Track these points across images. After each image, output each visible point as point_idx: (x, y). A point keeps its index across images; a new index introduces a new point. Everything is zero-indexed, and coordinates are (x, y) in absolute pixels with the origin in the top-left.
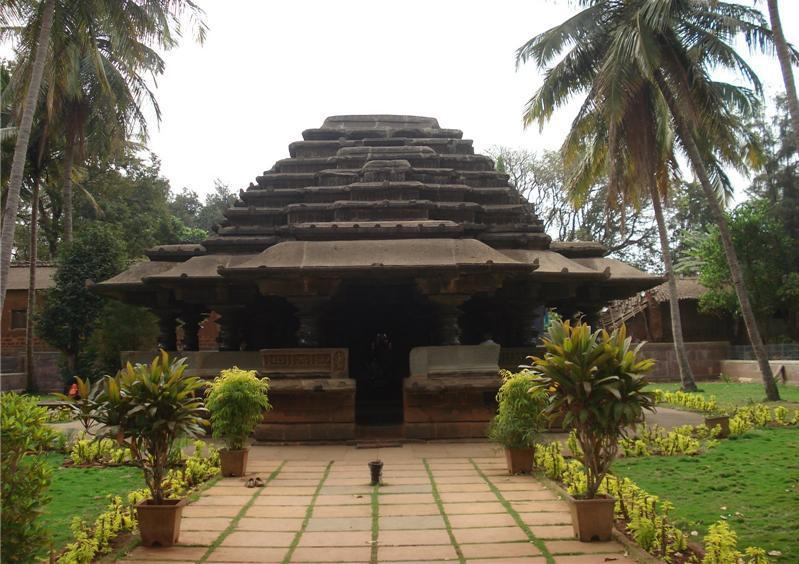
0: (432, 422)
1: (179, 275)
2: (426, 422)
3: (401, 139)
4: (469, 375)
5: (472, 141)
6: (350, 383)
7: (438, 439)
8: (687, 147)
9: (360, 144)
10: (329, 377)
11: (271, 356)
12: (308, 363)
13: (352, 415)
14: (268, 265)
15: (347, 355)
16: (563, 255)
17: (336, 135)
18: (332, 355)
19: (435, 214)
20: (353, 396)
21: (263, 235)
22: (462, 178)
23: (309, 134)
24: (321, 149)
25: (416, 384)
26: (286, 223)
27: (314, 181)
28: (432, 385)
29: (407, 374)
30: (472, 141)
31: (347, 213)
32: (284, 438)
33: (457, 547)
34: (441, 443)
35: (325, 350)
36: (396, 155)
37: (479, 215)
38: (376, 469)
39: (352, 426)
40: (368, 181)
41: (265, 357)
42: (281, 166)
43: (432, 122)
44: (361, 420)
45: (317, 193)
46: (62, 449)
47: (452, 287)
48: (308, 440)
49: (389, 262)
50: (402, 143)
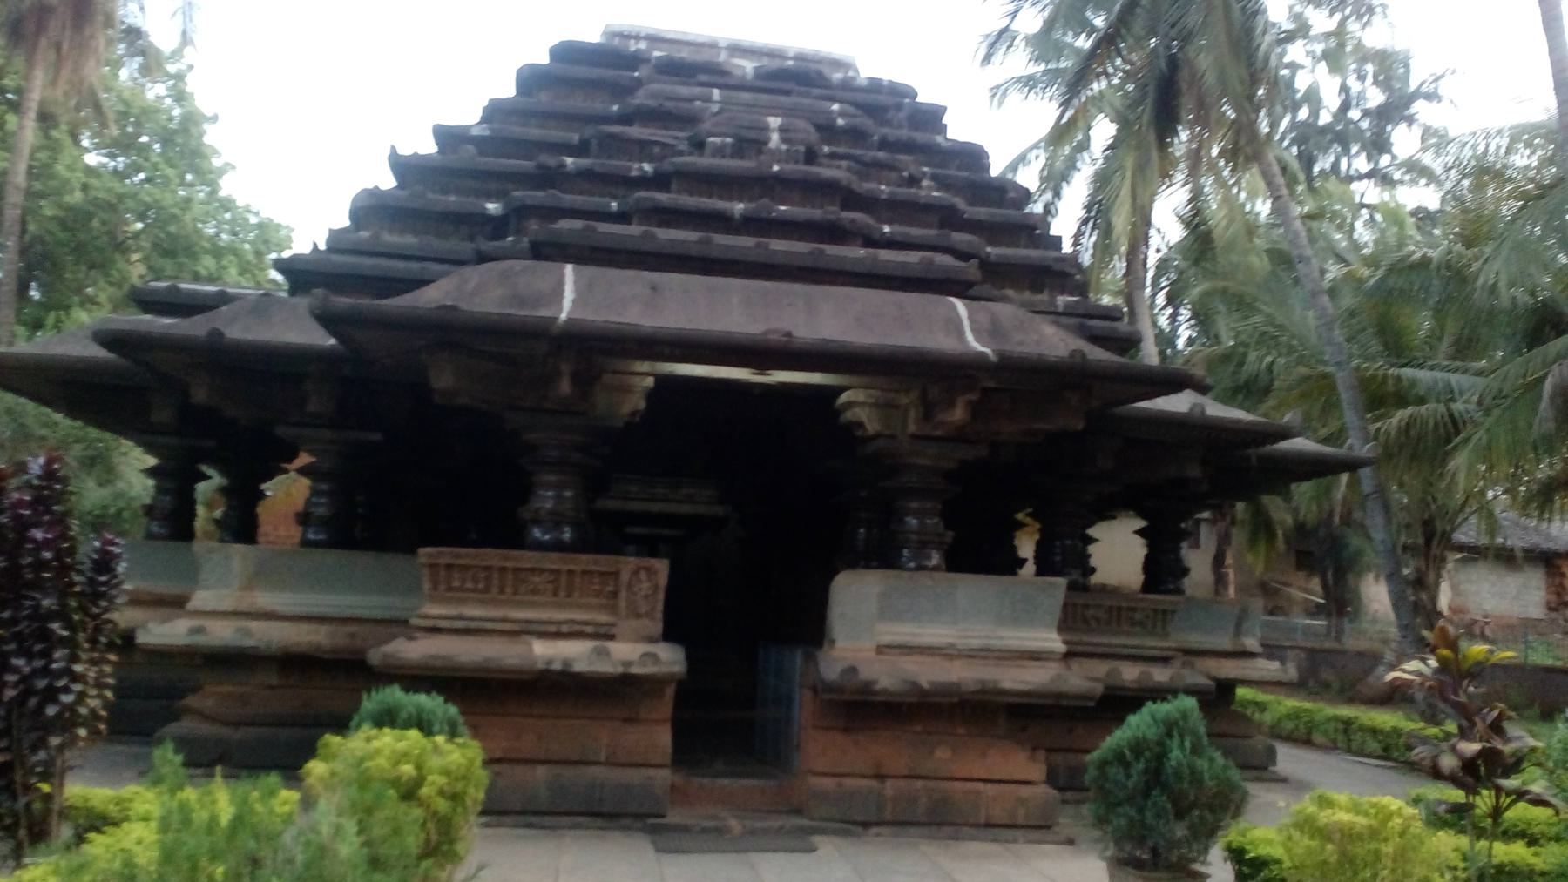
0: (881, 777)
2: (863, 776)
5: (945, 109)
6: (670, 659)
8: (1134, 402)
10: (611, 637)
11: (449, 567)
13: (664, 737)
15: (663, 580)
18: (625, 577)
20: (670, 691)
23: (566, 53)
25: (852, 670)
28: (886, 676)
30: (945, 109)
32: (602, 758)
34: (770, 49)
35: (603, 562)
39: (664, 776)
41: (433, 566)
45: (586, 175)
49: (703, 206)
50: (788, 93)
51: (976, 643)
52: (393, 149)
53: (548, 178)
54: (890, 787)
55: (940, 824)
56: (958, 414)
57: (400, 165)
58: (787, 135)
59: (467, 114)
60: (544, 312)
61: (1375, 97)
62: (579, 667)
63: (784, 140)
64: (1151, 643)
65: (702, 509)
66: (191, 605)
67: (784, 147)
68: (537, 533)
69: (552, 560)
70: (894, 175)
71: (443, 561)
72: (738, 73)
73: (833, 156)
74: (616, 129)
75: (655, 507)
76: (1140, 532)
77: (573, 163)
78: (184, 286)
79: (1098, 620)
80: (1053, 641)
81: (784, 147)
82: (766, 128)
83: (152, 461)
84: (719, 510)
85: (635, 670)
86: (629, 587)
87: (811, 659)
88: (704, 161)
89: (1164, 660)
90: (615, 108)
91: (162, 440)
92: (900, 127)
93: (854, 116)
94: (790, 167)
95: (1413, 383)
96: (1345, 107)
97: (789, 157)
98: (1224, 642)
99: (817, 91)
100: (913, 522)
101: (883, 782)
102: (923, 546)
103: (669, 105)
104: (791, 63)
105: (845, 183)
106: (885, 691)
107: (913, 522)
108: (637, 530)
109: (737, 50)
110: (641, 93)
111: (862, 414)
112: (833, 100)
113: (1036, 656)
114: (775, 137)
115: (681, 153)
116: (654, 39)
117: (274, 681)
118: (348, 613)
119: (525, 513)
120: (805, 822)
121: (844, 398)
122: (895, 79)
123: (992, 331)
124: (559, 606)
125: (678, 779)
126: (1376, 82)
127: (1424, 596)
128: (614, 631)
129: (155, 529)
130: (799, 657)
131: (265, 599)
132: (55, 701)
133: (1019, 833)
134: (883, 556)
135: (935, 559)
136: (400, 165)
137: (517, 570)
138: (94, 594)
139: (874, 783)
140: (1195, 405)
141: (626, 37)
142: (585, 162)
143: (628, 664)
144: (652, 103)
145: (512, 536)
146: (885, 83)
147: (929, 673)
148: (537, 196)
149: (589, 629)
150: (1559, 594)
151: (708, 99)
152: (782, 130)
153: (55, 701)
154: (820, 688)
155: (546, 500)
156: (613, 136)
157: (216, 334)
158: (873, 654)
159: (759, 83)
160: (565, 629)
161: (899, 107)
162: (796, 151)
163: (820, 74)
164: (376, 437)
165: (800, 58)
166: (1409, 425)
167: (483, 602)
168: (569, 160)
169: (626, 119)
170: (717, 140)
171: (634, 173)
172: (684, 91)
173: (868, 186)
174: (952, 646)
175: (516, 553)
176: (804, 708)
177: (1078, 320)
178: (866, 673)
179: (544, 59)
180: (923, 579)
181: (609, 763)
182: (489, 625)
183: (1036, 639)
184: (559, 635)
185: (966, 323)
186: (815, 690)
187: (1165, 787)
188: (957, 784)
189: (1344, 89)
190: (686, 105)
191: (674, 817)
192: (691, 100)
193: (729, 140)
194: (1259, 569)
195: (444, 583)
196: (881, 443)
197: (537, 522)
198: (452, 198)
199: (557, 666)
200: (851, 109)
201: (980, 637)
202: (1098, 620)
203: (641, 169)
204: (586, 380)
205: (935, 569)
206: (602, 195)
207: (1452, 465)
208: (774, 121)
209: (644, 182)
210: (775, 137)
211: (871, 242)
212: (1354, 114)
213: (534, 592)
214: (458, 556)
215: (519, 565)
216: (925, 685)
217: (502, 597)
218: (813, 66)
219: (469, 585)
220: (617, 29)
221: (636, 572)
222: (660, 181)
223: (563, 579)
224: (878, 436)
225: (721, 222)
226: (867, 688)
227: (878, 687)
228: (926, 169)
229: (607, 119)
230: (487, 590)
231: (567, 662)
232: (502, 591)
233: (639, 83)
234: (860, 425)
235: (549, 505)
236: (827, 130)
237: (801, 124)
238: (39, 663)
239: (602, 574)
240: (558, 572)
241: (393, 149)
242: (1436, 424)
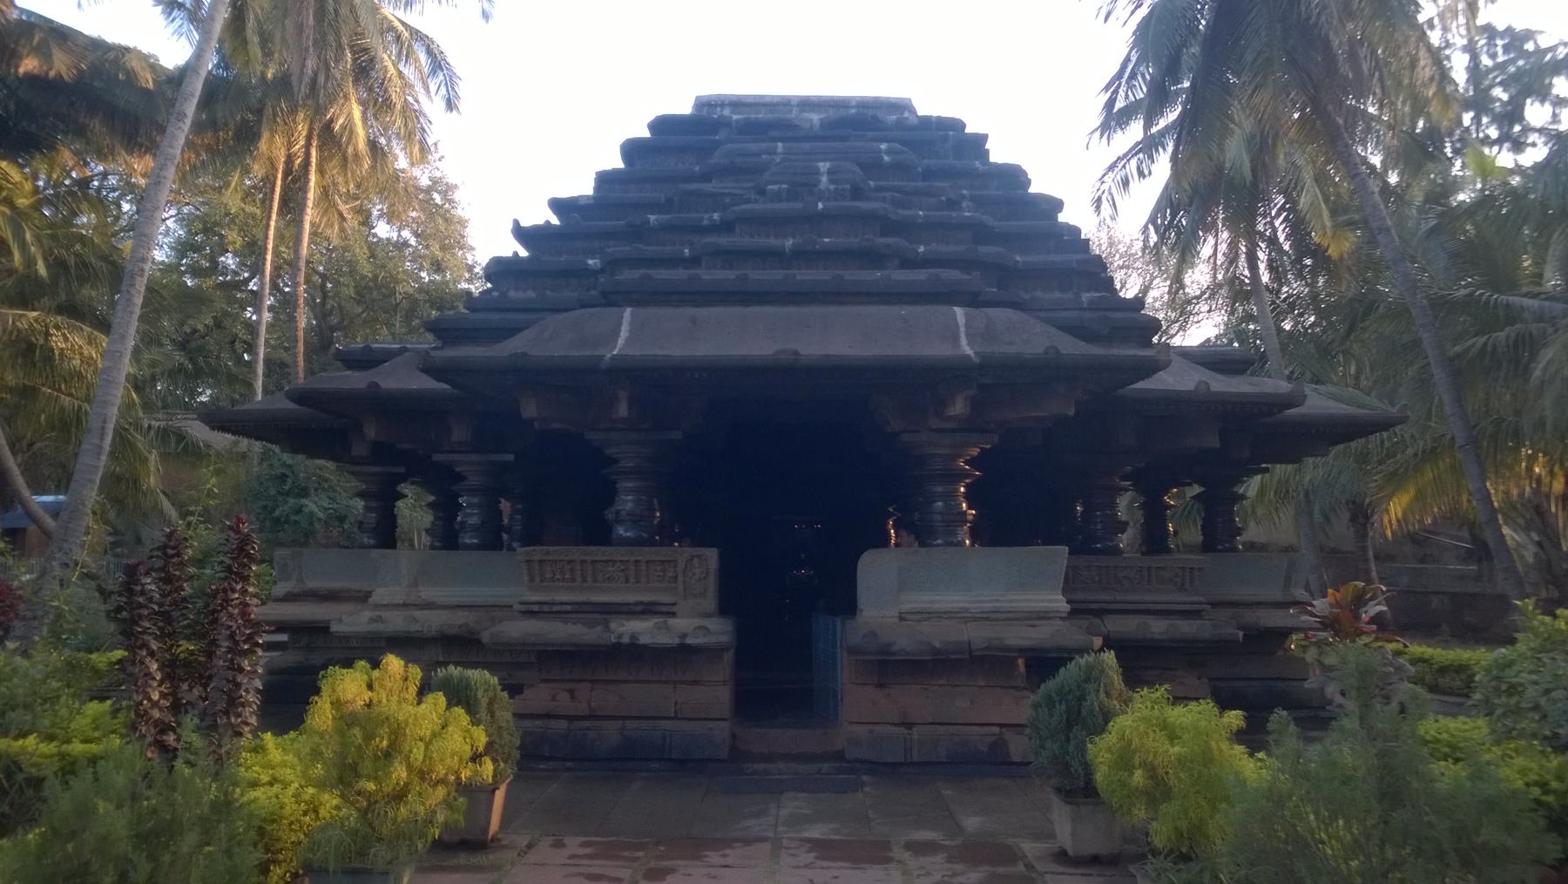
0: (909, 726)
10: (673, 615)
12: (627, 581)
16: (1206, 368)
18: (681, 565)
20: (729, 657)
23: (663, 125)
28: (903, 642)
29: (849, 607)
35: (662, 553)
36: (806, 275)
40: (772, 201)
43: (902, 106)
46: (1319, 647)
47: (958, 408)
50: (844, 139)
52: (516, 223)
53: (637, 233)
57: (522, 234)
59: (583, 186)
63: (831, 181)
66: (374, 599)
67: (832, 187)
68: (621, 531)
71: (537, 557)
73: (879, 189)
74: (694, 186)
77: (656, 220)
80: (1060, 603)
81: (832, 187)
82: (817, 172)
85: (689, 641)
88: (761, 206)
91: (365, 469)
94: (831, 204)
98: (1276, 595)
99: (870, 134)
101: (910, 729)
104: (853, 111)
113: (1044, 616)
114: (824, 179)
115: (748, 201)
119: (610, 515)
122: (944, 114)
128: (675, 609)
129: (437, 544)
130: (838, 621)
131: (428, 593)
134: (921, 533)
136: (522, 234)
137: (593, 562)
139: (903, 730)
140: (1200, 382)
142: (665, 217)
143: (684, 636)
145: (599, 533)
146: (934, 120)
147: (940, 635)
155: (627, 502)
157: (374, 386)
158: (897, 620)
161: (945, 139)
162: (843, 189)
163: (875, 118)
164: (511, 457)
168: (652, 218)
169: (706, 177)
170: (775, 187)
171: (706, 222)
172: (754, 147)
174: (966, 610)
179: (645, 133)
183: (1043, 601)
185: (962, 329)
192: (758, 155)
193: (785, 186)
201: (990, 601)
203: (710, 219)
208: (824, 166)
209: (714, 229)
210: (824, 179)
211: (908, 263)
214: (548, 553)
215: (596, 559)
216: (937, 645)
217: (585, 585)
218: (871, 112)
222: (727, 227)
225: (774, 256)
227: (895, 648)
228: (965, 192)
229: (692, 178)
230: (573, 580)
231: (633, 636)
232: (584, 580)
233: (718, 144)
235: (629, 506)
241: (516, 223)
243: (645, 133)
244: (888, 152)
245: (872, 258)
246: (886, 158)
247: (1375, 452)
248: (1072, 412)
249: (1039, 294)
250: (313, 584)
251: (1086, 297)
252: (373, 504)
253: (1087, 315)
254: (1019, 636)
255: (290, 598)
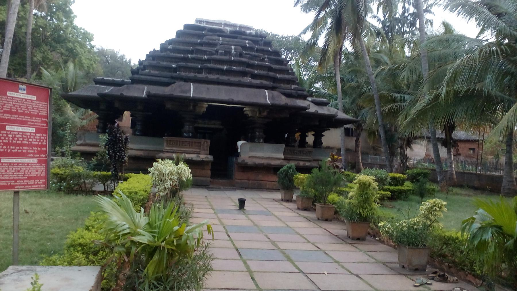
0: (249, 180)
1: (314, 111)
3: (236, 35)
4: (269, 158)
6: (211, 158)
7: (257, 188)
9: (214, 35)
10: (200, 154)
13: (209, 172)
14: (174, 94)
15: (209, 144)
17: (203, 29)
18: (202, 143)
19: (254, 76)
20: (210, 164)
21: (163, 77)
22: (266, 59)
23: (187, 27)
24: (193, 35)
25: (244, 161)
26: (373, 95)
27: (191, 52)
28: (250, 162)
31: (211, 71)
33: (232, 241)
37: (275, 80)
38: (242, 203)
39: (209, 179)
41: (167, 141)
42: (170, 42)
44: (213, 176)
45: (193, 59)
48: (198, 185)
50: (236, 38)
51: (267, 156)
54: (250, 182)
55: (259, 189)
56: (265, 114)
58: (236, 50)
60: (188, 95)
61: (412, 10)
62: (194, 159)
63: (235, 51)
64: (307, 158)
65: (217, 127)
69: (188, 140)
70: (259, 59)
71: (169, 139)
72: (226, 31)
73: (246, 54)
75: (206, 126)
76: (313, 135)
78: (105, 78)
79: (296, 153)
80: (282, 156)
81: (235, 53)
82: (232, 49)
83: (97, 116)
84: (221, 127)
85: (204, 160)
86: (203, 145)
87: (237, 159)
89: (309, 161)
90: (199, 41)
92: (261, 45)
93: (251, 44)
95: (396, 97)
96: (404, 12)
97: (235, 56)
99: (244, 37)
100: (257, 133)
102: (259, 138)
103: (210, 41)
104: (238, 29)
105: (247, 62)
106: (250, 164)
107: (257, 133)
108: (200, 131)
109: (226, 25)
110: (204, 38)
111: (248, 112)
112: (246, 39)
113: (279, 159)
114: (233, 51)
116: (208, 22)
117: (132, 162)
118: (147, 149)
120: (235, 187)
121: (245, 109)
123: (272, 98)
124: (190, 148)
125: (212, 180)
126: (413, 6)
127: (402, 151)
132: (124, 159)
133: (274, 190)
135: (262, 141)
137: (182, 141)
138: (125, 143)
141: (200, 21)
143: (202, 159)
144: (207, 41)
145: (180, 135)
147: (258, 161)
148: (183, 64)
149: (196, 152)
150: (457, 152)
151: (219, 40)
152: (235, 49)
153: (124, 159)
154: (238, 164)
155: (187, 128)
156: (199, 50)
159: (231, 35)
160: (191, 152)
163: (244, 32)
164: (151, 114)
165: (240, 27)
166: (391, 108)
167: (176, 147)
168: (189, 55)
170: (221, 51)
171: (203, 59)
173: (252, 62)
174: (263, 157)
175: (182, 138)
176: (235, 168)
177: (296, 91)
178: (246, 161)
179: (182, 28)
180: (258, 145)
181: (199, 176)
182: (169, 151)
184: (190, 153)
186: (237, 164)
187: (288, 177)
188: (263, 182)
189: (404, 7)
190: (214, 42)
191: (211, 186)
192: (215, 40)
194: (371, 143)
195: (169, 143)
196: (251, 118)
197: (185, 132)
198: (165, 63)
199: (190, 159)
200: (250, 42)
202: (296, 153)
204: (194, 106)
205: (262, 142)
206: (197, 63)
207: (398, 119)
208: (233, 47)
210: (233, 51)
212: (406, 15)
213: (185, 145)
219: (173, 144)
220: (199, 20)
221: (204, 142)
223: (191, 143)
224: (251, 117)
226: (246, 164)
230: (177, 145)
231: (192, 158)
234: (248, 114)
235: (187, 129)
236: (244, 48)
237: (239, 47)
238: (121, 154)
239: (198, 142)
240: (190, 142)
242: (397, 109)
243: (182, 28)
244: (248, 44)
245: (244, 74)
246: (248, 45)
247: (26, 234)
248: (288, 116)
249: (282, 85)
250: (88, 142)
251: (293, 87)
252: (102, 121)
253: (293, 91)
254: (274, 163)
255: (81, 145)
